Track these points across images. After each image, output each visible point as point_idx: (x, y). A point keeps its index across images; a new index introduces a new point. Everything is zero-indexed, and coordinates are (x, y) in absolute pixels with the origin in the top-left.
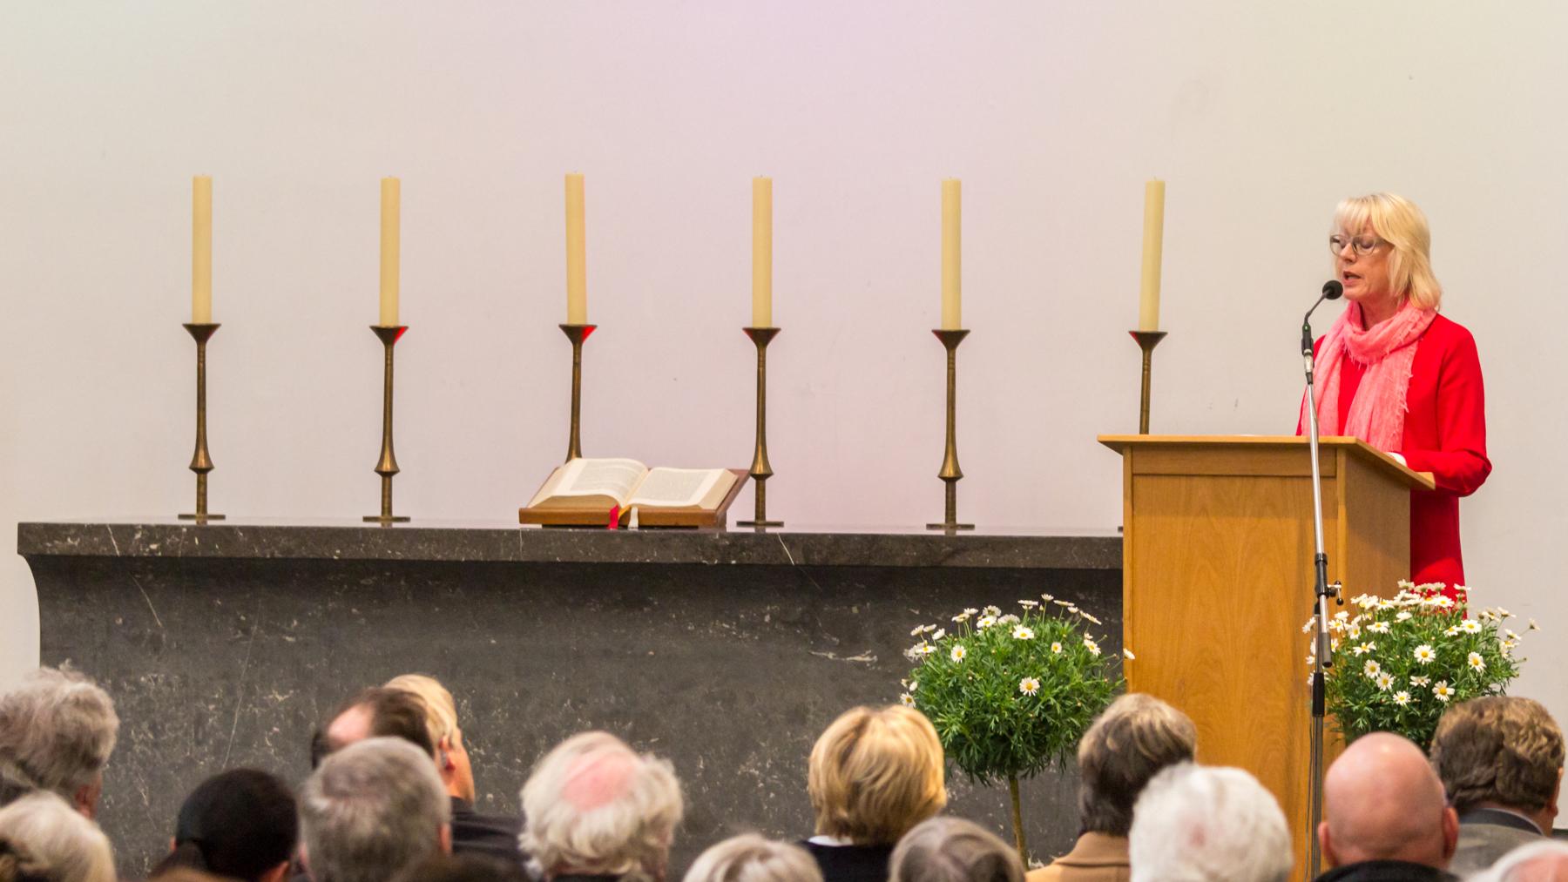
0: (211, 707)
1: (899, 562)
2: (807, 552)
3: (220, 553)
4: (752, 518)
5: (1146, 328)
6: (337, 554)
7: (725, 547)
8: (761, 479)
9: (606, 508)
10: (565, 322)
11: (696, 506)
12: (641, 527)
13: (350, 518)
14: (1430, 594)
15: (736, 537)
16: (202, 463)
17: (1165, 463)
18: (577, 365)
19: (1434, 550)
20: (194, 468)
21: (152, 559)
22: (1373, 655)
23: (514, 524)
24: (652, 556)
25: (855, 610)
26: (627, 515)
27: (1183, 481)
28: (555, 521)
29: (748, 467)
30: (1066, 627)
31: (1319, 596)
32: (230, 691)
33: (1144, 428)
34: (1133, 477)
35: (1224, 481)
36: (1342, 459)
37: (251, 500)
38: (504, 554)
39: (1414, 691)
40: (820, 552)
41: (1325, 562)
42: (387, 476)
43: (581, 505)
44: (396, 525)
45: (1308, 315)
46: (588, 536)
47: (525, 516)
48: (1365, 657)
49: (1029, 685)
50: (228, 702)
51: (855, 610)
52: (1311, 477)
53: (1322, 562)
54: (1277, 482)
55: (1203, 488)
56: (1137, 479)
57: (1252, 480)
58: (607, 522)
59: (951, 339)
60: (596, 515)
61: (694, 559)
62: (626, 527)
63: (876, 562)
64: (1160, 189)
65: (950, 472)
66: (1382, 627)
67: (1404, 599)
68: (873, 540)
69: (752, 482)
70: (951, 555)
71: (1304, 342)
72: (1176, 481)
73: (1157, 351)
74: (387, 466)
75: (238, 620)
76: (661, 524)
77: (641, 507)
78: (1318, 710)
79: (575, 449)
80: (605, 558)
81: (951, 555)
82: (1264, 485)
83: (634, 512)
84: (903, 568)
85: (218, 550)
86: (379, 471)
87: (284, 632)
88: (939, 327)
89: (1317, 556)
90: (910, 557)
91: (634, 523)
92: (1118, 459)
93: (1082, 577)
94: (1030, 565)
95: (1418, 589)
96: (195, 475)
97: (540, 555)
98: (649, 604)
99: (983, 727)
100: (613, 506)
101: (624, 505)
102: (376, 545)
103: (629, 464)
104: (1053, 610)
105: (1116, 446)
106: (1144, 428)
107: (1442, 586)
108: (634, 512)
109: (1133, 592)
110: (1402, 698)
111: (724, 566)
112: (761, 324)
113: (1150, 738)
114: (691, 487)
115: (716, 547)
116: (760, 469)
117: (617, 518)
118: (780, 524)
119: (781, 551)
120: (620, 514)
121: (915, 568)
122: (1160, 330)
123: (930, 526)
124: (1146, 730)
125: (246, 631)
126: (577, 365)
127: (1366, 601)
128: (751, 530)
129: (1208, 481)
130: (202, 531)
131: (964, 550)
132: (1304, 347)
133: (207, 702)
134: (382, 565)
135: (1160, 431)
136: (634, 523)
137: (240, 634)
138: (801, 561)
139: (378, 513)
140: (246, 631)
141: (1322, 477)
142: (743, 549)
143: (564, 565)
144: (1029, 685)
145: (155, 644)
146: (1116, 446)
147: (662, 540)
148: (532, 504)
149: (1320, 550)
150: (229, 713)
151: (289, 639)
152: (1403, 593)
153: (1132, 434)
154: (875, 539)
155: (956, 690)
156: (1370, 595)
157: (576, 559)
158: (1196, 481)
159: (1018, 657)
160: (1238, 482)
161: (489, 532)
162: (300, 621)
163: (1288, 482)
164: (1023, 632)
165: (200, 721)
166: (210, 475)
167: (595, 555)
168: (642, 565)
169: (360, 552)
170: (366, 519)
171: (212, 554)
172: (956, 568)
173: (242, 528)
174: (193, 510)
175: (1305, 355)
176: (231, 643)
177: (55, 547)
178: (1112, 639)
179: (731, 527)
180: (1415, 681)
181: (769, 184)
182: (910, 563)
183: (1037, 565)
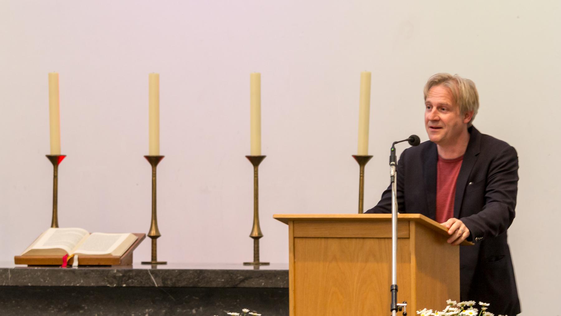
1: (214, 285)
2: (164, 280)
4: (149, 259)
5: (361, 153)
7: (120, 277)
8: (154, 238)
9: (61, 255)
10: (49, 154)
11: (109, 254)
12: (79, 266)
14: (466, 308)
15: (139, 271)
17: (312, 231)
24: (80, 282)
25: (194, 311)
26: (72, 259)
27: (323, 240)
28: (34, 262)
29: (147, 233)
31: (392, 310)
34: (294, 239)
35: (346, 241)
36: (413, 227)
40: (171, 280)
41: (396, 290)
43: (41, 254)
45: (396, 143)
46: (44, 271)
47: (18, 260)
51: (194, 311)
52: (391, 238)
53: (394, 290)
54: (377, 241)
55: (334, 245)
56: (296, 240)
57: (362, 240)
58: (61, 263)
59: (256, 160)
60: (56, 260)
61: (103, 284)
62: (71, 266)
63: (201, 285)
64: (369, 76)
65: (256, 234)
67: (448, 312)
68: (200, 273)
69: (148, 241)
70: (243, 281)
71: (391, 157)
72: (318, 241)
73: (368, 166)
76: (90, 264)
77: (79, 255)
79: (55, 223)
80: (54, 284)
81: (243, 281)
82: (368, 242)
83: (76, 257)
84: (216, 288)
88: (249, 154)
89: (392, 286)
90: (220, 282)
91: (75, 264)
92: (285, 228)
95: (459, 304)
97: (21, 282)
98: (83, 308)
100: (65, 254)
101: (70, 254)
103: (78, 231)
105: (285, 220)
107: (473, 303)
108: (76, 257)
109: (295, 308)
111: (119, 287)
114: (108, 244)
115: (114, 277)
116: (153, 233)
117: (67, 261)
118: (165, 263)
119: (150, 279)
120: (68, 258)
121: (224, 288)
122: (369, 154)
123: (245, 264)
128: (149, 267)
129: (337, 241)
132: (391, 161)
134: (152, 288)
136: (75, 264)
138: (161, 285)
139: (251, 260)
141: (398, 238)
142: (130, 278)
143: (33, 287)
146: (285, 220)
147: (86, 273)
148: (20, 253)
149: (394, 283)
152: (448, 308)
154: (201, 272)
156: (428, 309)
157: (38, 284)
158: (330, 241)
160: (354, 241)
163: (383, 241)
167: (48, 282)
168: (75, 288)
172: (244, 288)
175: (391, 165)
179: (137, 265)
181: (157, 77)
182: (220, 286)
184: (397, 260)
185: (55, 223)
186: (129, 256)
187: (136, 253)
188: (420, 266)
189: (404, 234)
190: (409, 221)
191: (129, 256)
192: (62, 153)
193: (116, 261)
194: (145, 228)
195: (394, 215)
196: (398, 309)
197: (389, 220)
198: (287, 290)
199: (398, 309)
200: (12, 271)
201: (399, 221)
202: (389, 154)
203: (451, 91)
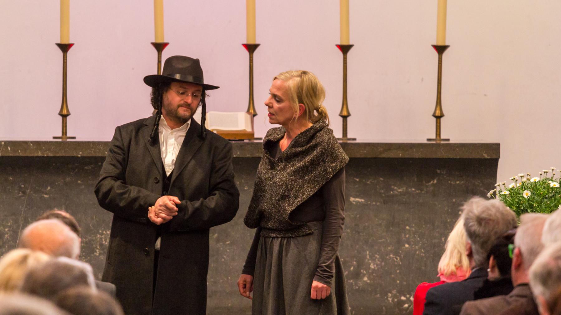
0: (6, 230)
3: (21, 154)
4: (60, 135)
13: (422, 139)
16: (65, 112)
20: (61, 114)
23: (426, 142)
32: (16, 221)
38: (392, 154)
44: (68, 140)
50: (15, 227)
59: (251, 48)
65: (438, 113)
74: (345, 113)
75: (20, 187)
86: (434, 116)
87: (43, 193)
94: (421, 156)
96: (434, 119)
102: (100, 150)
112: (440, 44)
125: (24, 193)
128: (60, 140)
131: (389, 149)
133: (5, 227)
137: (21, 194)
140: (24, 193)
147: (241, 146)
151: (46, 196)
161: (26, 143)
162: (52, 187)
166: (68, 118)
170: (54, 138)
171: (17, 154)
173: (32, 142)
174: (60, 135)
176: (16, 199)
183: (424, 156)
192: (257, 43)
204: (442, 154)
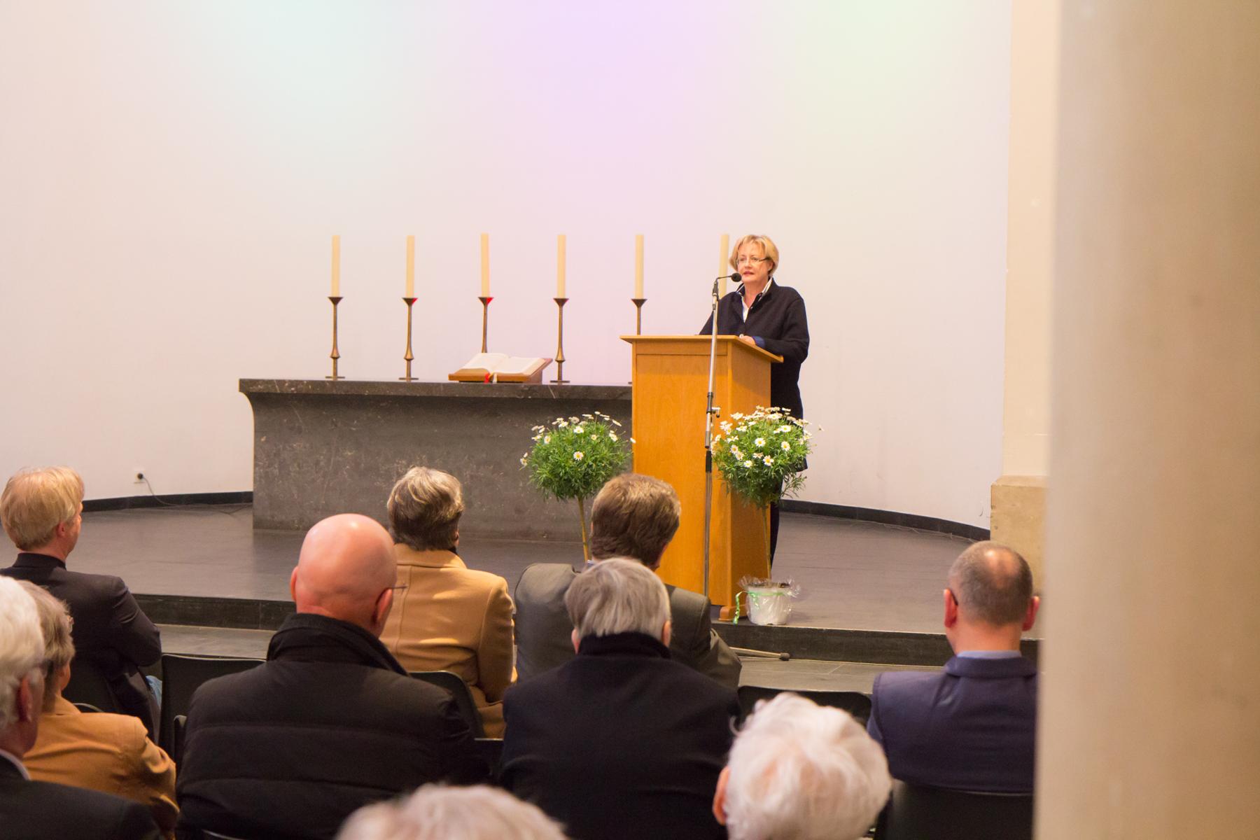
1: (599, 397)
6: (367, 393)
8: (560, 362)
9: (483, 374)
17: (651, 349)
18: (485, 314)
19: (785, 393)
21: (293, 395)
22: (736, 443)
23: (446, 380)
24: (496, 395)
30: (602, 427)
33: (639, 332)
34: (637, 356)
36: (730, 346)
37: (352, 372)
38: (435, 394)
39: (756, 460)
42: (335, 359)
47: (451, 377)
48: (730, 444)
49: (578, 456)
66: (744, 429)
68: (281, 383)
76: (505, 381)
78: (708, 468)
79: (485, 350)
85: (318, 391)
90: (604, 396)
91: (495, 380)
92: (630, 346)
93: (612, 403)
99: (557, 475)
104: (600, 419)
106: (639, 332)
110: (748, 464)
111: (525, 399)
113: (420, 491)
117: (489, 378)
124: (417, 486)
126: (485, 314)
127: (737, 416)
130: (334, 384)
134: (385, 398)
135: (645, 334)
136: (495, 380)
144: (578, 456)
145: (300, 431)
148: (453, 372)
150: (329, 460)
153: (634, 335)
155: (546, 459)
159: (576, 442)
164: (579, 430)
165: (317, 463)
167: (472, 394)
169: (376, 392)
177: (254, 389)
178: (625, 432)
180: (756, 455)
184: (713, 375)
185: (485, 350)
186: (539, 374)
187: (544, 372)
188: (736, 378)
189: (723, 351)
190: (726, 341)
191: (539, 374)
193: (527, 378)
194: (553, 354)
195: (714, 337)
196: (712, 412)
197: (710, 341)
198: (630, 402)
199: (712, 412)
200: (444, 385)
201: (719, 341)
202: (712, 287)
203: (655, 514)
204: (402, 392)
